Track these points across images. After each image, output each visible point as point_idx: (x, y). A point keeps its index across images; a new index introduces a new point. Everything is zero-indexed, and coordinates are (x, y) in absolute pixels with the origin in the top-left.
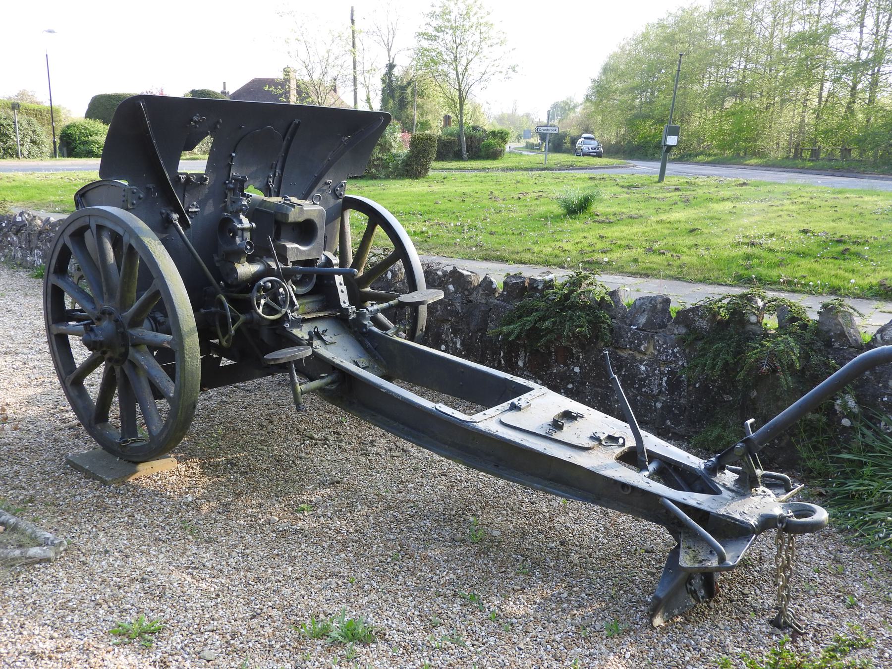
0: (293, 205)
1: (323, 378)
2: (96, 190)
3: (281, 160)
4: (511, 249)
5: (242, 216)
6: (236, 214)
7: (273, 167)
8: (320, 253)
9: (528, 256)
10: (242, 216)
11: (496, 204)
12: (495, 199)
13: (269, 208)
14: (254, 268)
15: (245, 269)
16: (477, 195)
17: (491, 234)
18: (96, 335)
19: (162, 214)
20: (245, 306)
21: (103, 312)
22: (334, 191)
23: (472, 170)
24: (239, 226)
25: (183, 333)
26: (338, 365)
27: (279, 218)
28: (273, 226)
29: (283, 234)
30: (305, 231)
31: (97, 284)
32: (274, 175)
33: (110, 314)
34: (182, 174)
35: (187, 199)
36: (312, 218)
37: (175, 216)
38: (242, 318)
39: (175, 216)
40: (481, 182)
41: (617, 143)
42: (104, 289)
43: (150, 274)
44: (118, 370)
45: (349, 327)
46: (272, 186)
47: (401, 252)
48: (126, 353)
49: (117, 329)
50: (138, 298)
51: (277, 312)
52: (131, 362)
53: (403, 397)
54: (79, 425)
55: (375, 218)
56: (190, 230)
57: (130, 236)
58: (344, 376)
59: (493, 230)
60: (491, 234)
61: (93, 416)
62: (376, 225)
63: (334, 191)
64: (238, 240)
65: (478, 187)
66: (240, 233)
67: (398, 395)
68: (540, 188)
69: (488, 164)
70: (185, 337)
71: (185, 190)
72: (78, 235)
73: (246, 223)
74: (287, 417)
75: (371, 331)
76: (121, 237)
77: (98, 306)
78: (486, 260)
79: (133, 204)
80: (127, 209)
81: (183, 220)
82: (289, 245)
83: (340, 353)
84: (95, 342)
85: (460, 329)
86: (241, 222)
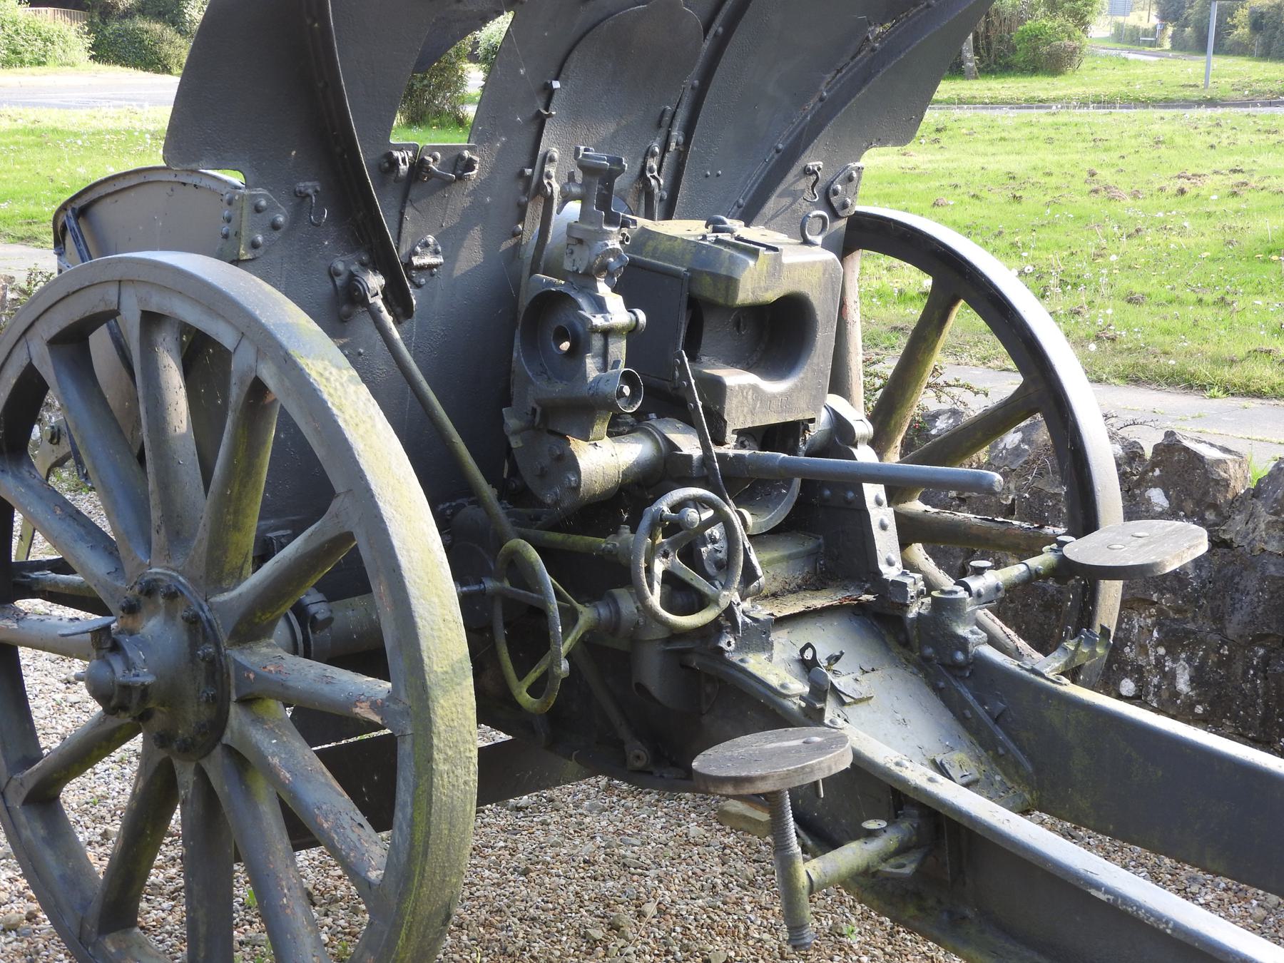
0: (751, 250)
1: (871, 834)
2: (108, 200)
3: (687, 100)
4: (1210, 349)
5: (603, 288)
6: (586, 279)
7: (662, 123)
8: (817, 402)
9: (1265, 373)
10: (603, 288)
11: (1115, 208)
12: (1109, 192)
13: (670, 255)
15: (603, 458)
16: (1052, 181)
17: (1132, 300)
18: (129, 665)
19: (333, 274)
20: (603, 577)
21: (149, 590)
22: (827, 194)
23: (994, 104)
24: (598, 321)
25: (431, 679)
26: (917, 789)
27: (706, 290)
28: (697, 315)
29: (705, 340)
30: (780, 332)
31: (131, 503)
32: (665, 148)
33: (172, 596)
34: (400, 148)
35: (408, 227)
36: (803, 288)
37: (375, 281)
38: (587, 615)
39: (375, 281)
40: (1050, 141)
42: (155, 515)
43: (315, 480)
44: (186, 777)
45: (906, 644)
46: (658, 183)
47: (1042, 393)
48: (219, 724)
49: (194, 646)
50: (262, 556)
51: (698, 602)
52: (231, 752)
53: (1178, 927)
54: (31, 917)
55: (955, 279)
57: (260, 354)
58: (939, 829)
59: (1137, 288)
60: (1132, 300)
61: (95, 909)
62: (954, 302)
63: (827, 194)
64: (591, 366)
65: (1047, 157)
66: (597, 342)
67: (1159, 917)
68: (1231, 161)
69: (1038, 86)
70: (436, 692)
71: (404, 200)
72: (72, 342)
73: (617, 312)
74: (662, 912)
75: (981, 663)
76: (224, 356)
77: (129, 567)
78: (1136, 381)
79: (255, 245)
80: (236, 262)
81: (397, 297)
82: (735, 378)
83: (887, 728)
84: (126, 688)
85: (1188, 633)
86: (600, 306)
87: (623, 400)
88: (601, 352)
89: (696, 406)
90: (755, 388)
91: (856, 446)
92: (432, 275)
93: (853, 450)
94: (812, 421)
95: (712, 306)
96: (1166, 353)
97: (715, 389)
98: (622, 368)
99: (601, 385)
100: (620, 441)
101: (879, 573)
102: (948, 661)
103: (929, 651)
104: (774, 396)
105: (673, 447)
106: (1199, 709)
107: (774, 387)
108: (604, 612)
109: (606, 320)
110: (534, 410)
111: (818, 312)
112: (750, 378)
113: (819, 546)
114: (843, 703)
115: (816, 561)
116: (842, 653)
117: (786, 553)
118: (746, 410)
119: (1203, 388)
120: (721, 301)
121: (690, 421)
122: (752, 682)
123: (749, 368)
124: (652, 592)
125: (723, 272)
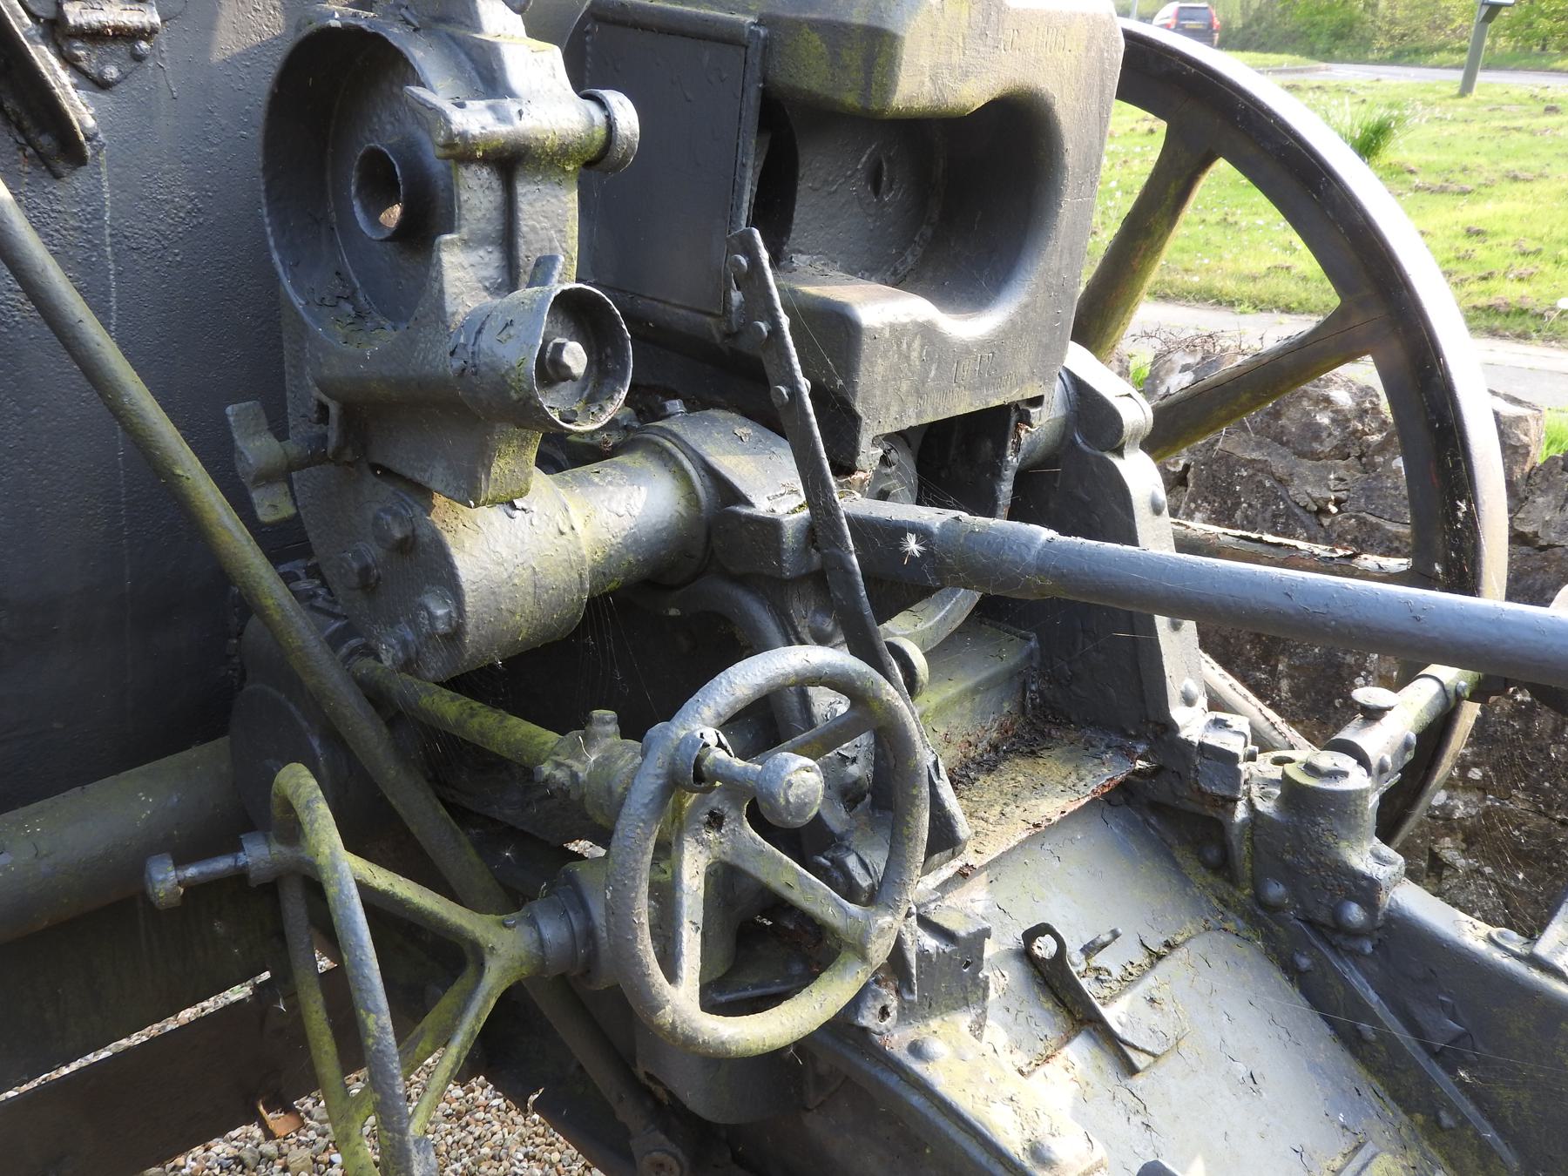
14: (622, 507)
15: (535, 538)
24: (474, 120)
27: (811, 74)
29: (802, 213)
41: (1246, 27)
45: (1223, 867)
56: (98, 183)
62: (1206, 163)
64: (462, 272)
66: (476, 194)
78: (1165, 298)
82: (881, 308)
86: (487, 76)
87: (566, 388)
88: (493, 227)
89: (795, 393)
90: (927, 332)
91: (1119, 452)
92: (138, 58)
93: (1117, 461)
94: (1037, 401)
95: (828, 118)
96: (1187, 271)
97: (833, 333)
98: (564, 279)
99: (486, 341)
100: (584, 482)
101: (1170, 727)
102: (1323, 916)
103: (1276, 891)
104: (966, 349)
105: (727, 492)
106: (1475, 774)
107: (969, 327)
108: (553, 931)
109: (503, 118)
110: (323, 409)
111: (1069, 145)
112: (912, 308)
113: (1030, 656)
114: (1132, 1070)
115: (1024, 687)
116: (1115, 935)
117: (970, 683)
118: (905, 386)
119: (1231, 304)
120: (851, 99)
121: (774, 419)
122: (953, 1131)
123: (901, 280)
124: (672, 976)
125: (857, 17)
